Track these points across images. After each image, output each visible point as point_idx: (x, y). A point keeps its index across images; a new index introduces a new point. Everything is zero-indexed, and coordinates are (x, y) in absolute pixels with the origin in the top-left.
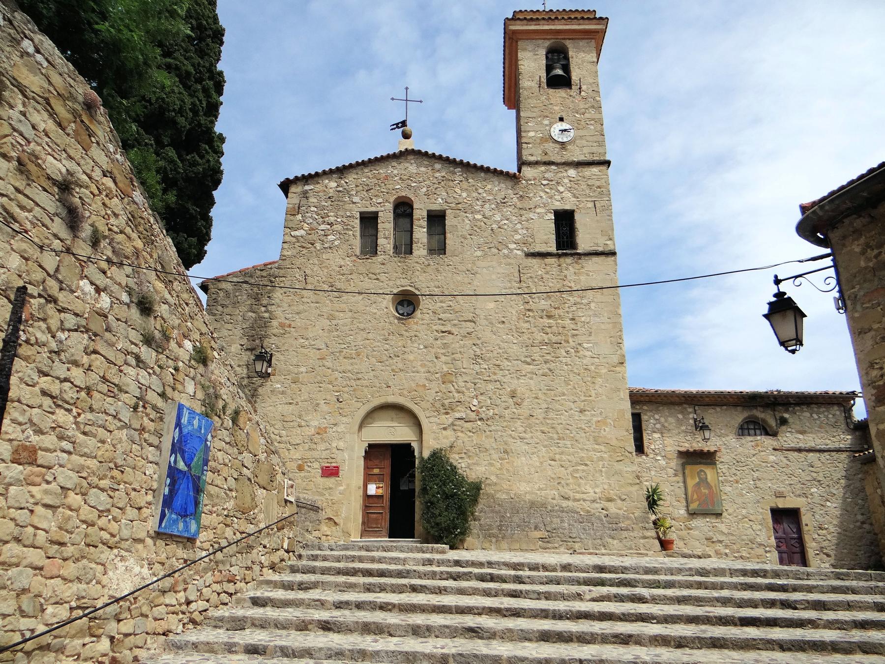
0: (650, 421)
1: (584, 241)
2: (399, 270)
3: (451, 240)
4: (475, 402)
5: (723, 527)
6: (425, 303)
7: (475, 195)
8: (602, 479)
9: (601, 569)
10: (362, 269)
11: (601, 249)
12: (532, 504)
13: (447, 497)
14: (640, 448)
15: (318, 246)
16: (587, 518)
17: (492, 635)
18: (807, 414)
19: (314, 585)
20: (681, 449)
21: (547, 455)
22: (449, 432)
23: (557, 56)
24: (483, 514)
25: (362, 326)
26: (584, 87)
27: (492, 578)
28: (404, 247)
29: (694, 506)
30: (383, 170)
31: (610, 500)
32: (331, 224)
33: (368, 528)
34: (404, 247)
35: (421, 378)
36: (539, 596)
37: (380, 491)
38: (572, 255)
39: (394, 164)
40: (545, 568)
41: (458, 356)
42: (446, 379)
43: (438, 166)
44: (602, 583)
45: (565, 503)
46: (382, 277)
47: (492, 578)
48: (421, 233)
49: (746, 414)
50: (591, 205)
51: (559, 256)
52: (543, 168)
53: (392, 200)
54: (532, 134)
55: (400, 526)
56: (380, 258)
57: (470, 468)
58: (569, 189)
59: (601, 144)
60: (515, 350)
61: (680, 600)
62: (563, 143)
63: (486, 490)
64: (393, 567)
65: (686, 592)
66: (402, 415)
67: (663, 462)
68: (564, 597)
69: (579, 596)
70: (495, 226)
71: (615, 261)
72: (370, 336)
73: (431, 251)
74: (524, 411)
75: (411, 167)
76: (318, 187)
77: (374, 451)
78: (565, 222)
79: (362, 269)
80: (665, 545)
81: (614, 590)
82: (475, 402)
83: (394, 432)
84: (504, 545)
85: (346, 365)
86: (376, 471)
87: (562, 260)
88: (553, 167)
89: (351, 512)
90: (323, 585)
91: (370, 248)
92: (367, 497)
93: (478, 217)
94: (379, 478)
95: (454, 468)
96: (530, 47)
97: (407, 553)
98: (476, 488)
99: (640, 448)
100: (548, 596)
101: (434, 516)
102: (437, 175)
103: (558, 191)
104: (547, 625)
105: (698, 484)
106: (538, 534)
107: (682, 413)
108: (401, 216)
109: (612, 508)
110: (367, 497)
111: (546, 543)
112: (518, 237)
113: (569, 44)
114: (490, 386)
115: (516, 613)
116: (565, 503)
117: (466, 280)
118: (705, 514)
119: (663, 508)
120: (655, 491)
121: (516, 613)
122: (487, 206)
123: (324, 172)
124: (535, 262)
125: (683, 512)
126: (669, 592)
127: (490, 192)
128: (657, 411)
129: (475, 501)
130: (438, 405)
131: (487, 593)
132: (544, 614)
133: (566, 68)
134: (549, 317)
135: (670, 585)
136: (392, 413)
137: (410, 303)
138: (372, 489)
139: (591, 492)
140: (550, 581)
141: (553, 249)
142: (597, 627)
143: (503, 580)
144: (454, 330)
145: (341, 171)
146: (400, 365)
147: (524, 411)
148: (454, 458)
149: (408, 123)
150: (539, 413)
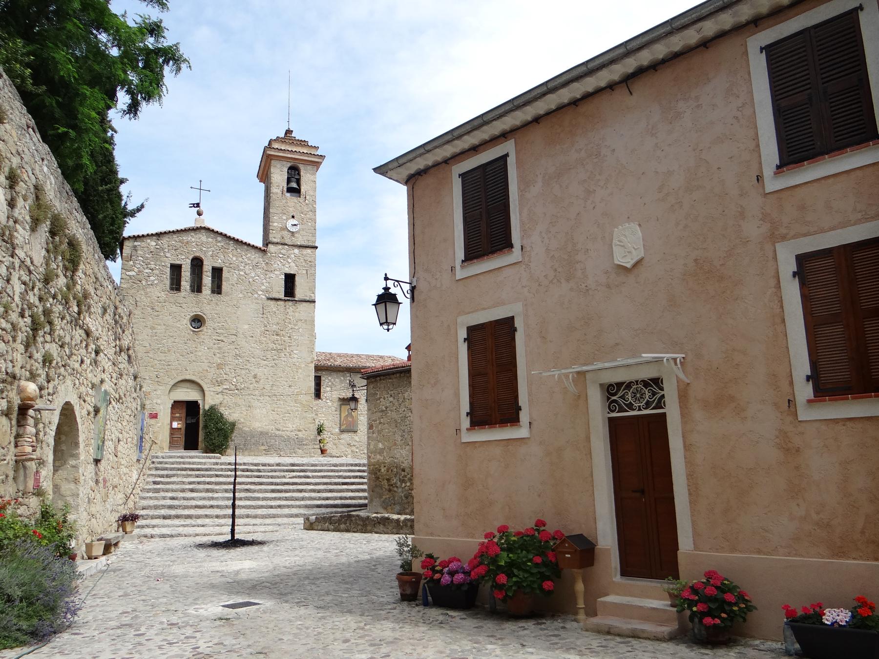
0: (326, 381)
1: (299, 293)
2: (194, 302)
3: (225, 286)
4: (235, 380)
5: (357, 438)
6: (209, 323)
7: (240, 259)
8: (297, 420)
9: (293, 465)
10: (172, 300)
11: (308, 299)
12: (261, 433)
13: (219, 430)
14: (318, 394)
15: (144, 282)
16: (288, 439)
17: (254, 491)
19: (174, 476)
20: (341, 397)
21: (268, 406)
22: (220, 396)
23: (294, 173)
24: (236, 438)
25: (171, 334)
27: (248, 470)
28: (197, 287)
29: (343, 427)
30: (185, 238)
31: (299, 431)
32: (152, 270)
33: (172, 445)
34: (197, 287)
35: (205, 366)
36: (268, 477)
37: (180, 426)
39: (193, 234)
40: (269, 465)
41: (226, 354)
42: (219, 366)
43: (219, 239)
44: (293, 471)
45: (277, 432)
46: (184, 306)
47: (248, 470)
48: (207, 280)
50: (304, 272)
51: (285, 301)
52: (280, 247)
53: (191, 258)
54: (275, 224)
55: (191, 443)
56: (183, 294)
57: (230, 414)
58: (294, 261)
59: (314, 235)
60: (258, 352)
61: (323, 477)
62: (293, 232)
63: (238, 426)
64: (203, 467)
65: (325, 474)
66: (193, 385)
67: (330, 404)
68: (278, 477)
69: (284, 477)
70: (251, 280)
72: (176, 341)
73: (213, 292)
74: (260, 386)
75: (203, 237)
76: (143, 244)
77: (176, 404)
78: (290, 280)
79: (172, 300)
80: (323, 452)
81: (298, 474)
82: (235, 380)
83: (188, 394)
84: (246, 453)
85: (162, 357)
86: (178, 415)
89: (164, 437)
90: (177, 475)
91: (176, 285)
92: (172, 429)
93: (242, 273)
94: (179, 419)
95: (222, 415)
96: (278, 166)
97: (197, 458)
98: (233, 425)
99: (318, 394)
100: (272, 477)
101: (211, 439)
102: (219, 244)
104: (273, 487)
106: (263, 448)
108: (197, 275)
109: (300, 435)
110: (172, 429)
111: (267, 452)
112: (263, 287)
113: (301, 167)
114: (243, 372)
115: (261, 484)
116: (277, 432)
117: (233, 311)
118: (348, 431)
119: (325, 435)
120: (321, 426)
121: (261, 484)
123: (148, 235)
124: (272, 302)
125: (337, 430)
126: (319, 474)
127: (249, 259)
128: (330, 375)
129: (232, 431)
130: (214, 381)
131: (247, 477)
132: (272, 484)
133: (298, 182)
134: (277, 335)
135: (320, 471)
136: (188, 385)
137: (199, 321)
138: (175, 425)
139: (291, 426)
140: (272, 471)
141: (282, 296)
142: (291, 487)
143: (252, 471)
144: (224, 339)
145: (159, 235)
146: (194, 358)
147: (260, 386)
148: (223, 410)
149: (201, 205)
150: (268, 387)
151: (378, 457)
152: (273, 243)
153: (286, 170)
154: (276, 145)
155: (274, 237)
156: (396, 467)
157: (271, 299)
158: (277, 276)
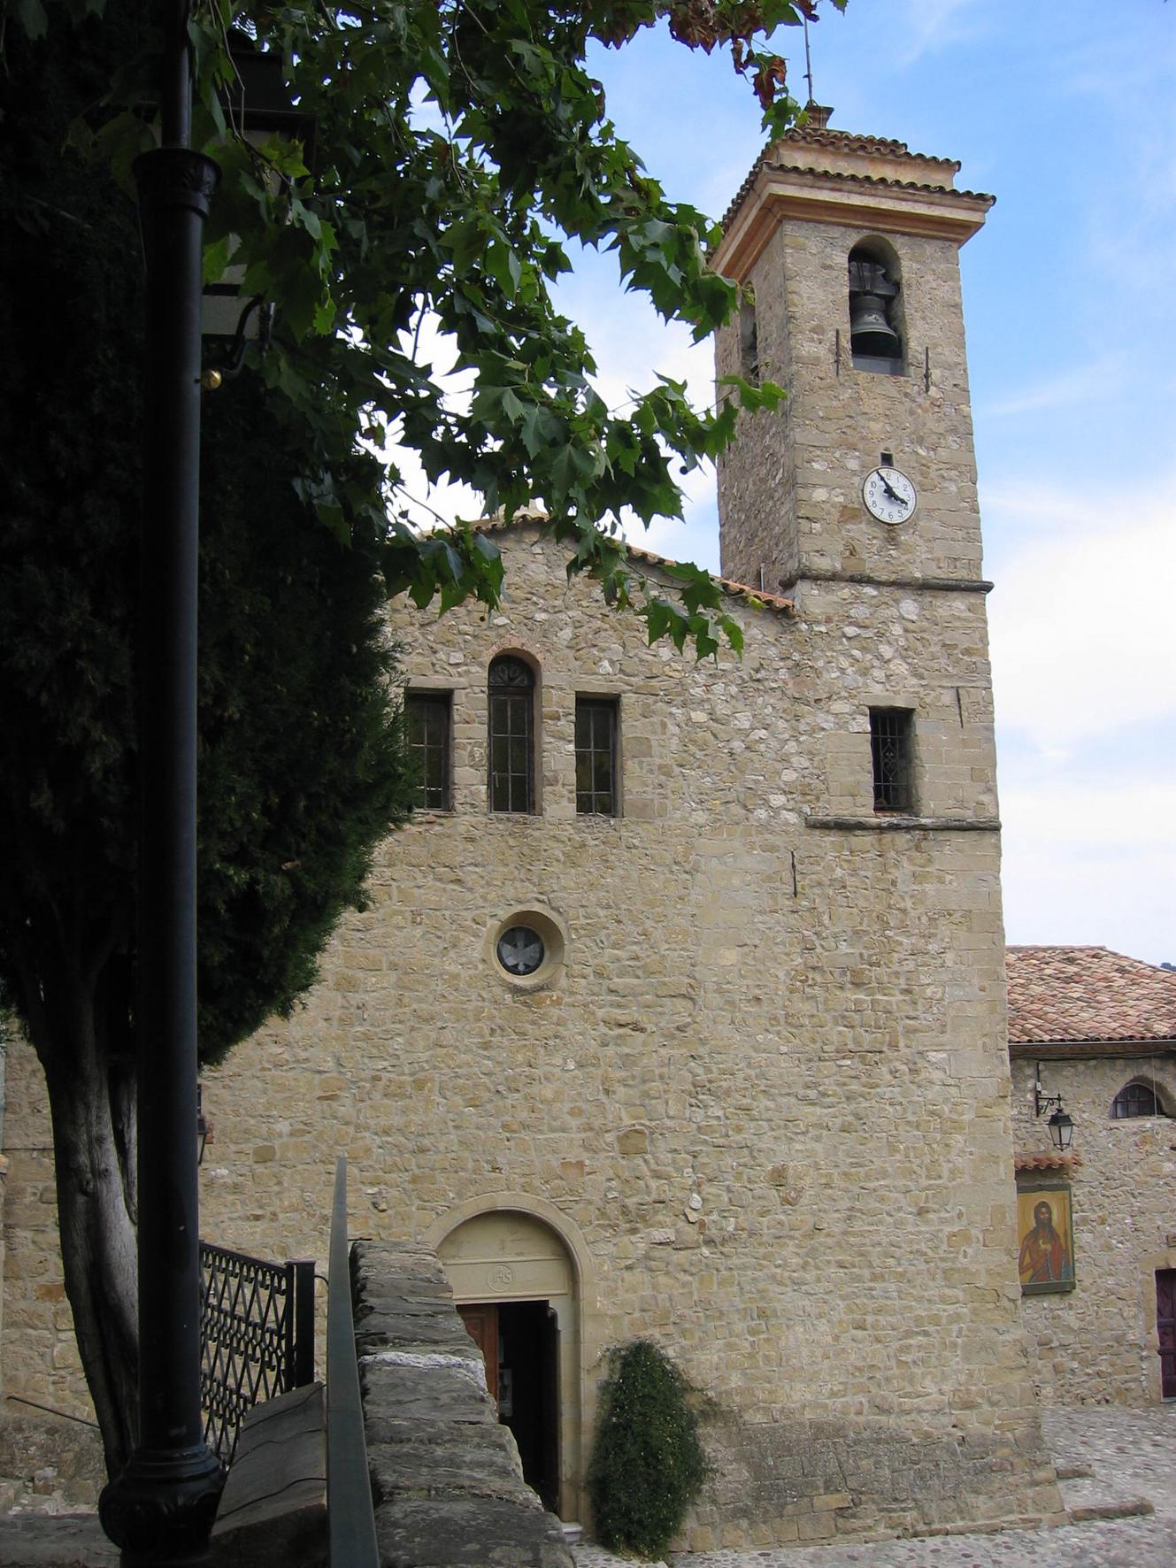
26: (936, 374)
38: (908, 829)
52: (846, 592)
54: (820, 494)
78: (891, 730)
87: (887, 837)
88: (870, 591)
93: (699, 716)
103: (879, 657)
112: (789, 776)
122: (719, 688)
124: (832, 838)
150: (833, 1222)
153: (842, 259)
157: (825, 826)
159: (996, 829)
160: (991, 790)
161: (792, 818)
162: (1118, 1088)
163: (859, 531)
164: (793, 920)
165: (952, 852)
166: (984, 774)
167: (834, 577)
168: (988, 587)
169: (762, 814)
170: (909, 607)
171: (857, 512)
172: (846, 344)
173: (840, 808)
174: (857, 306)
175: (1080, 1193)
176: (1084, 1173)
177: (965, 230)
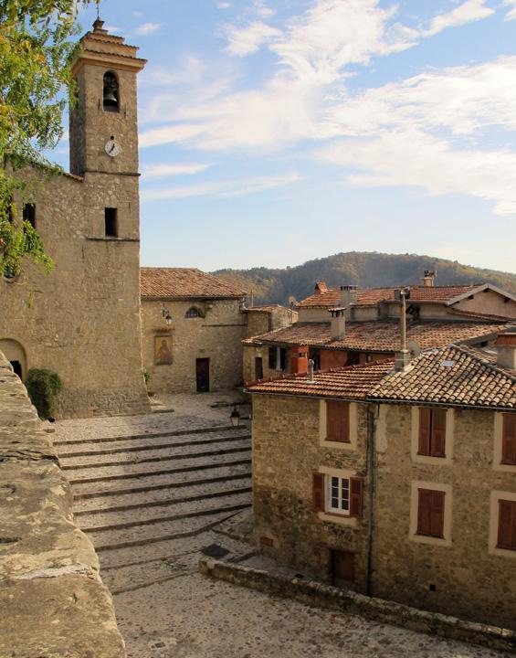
1: (122, 231)
8: (125, 376)
18: (221, 305)
26: (128, 113)
38: (115, 240)
49: (191, 306)
51: (107, 241)
52: (99, 175)
54: (93, 148)
71: (183, 391)
78: (111, 215)
87: (109, 243)
88: (106, 176)
93: (57, 210)
103: (108, 194)
105: (161, 348)
106: (92, 408)
107: (156, 306)
112: (82, 226)
113: (119, 73)
122: (63, 202)
124: (93, 243)
127: (64, 192)
133: (116, 95)
144: (41, 290)
150: (92, 341)
151: (267, 481)
152: (90, 172)
153: (102, 77)
154: (90, 45)
155: (92, 164)
156: (291, 496)
157: (91, 240)
158: (97, 212)
159: (138, 241)
160: (138, 231)
161: (82, 237)
162: (187, 309)
163: (103, 158)
164: (83, 265)
165: (127, 247)
166: (136, 225)
167: (96, 171)
168: (139, 175)
169: (74, 236)
170: (117, 180)
171: (102, 153)
172: (102, 103)
173: (95, 235)
174: (106, 91)
175: (175, 338)
176: (177, 332)
177: (138, 69)
